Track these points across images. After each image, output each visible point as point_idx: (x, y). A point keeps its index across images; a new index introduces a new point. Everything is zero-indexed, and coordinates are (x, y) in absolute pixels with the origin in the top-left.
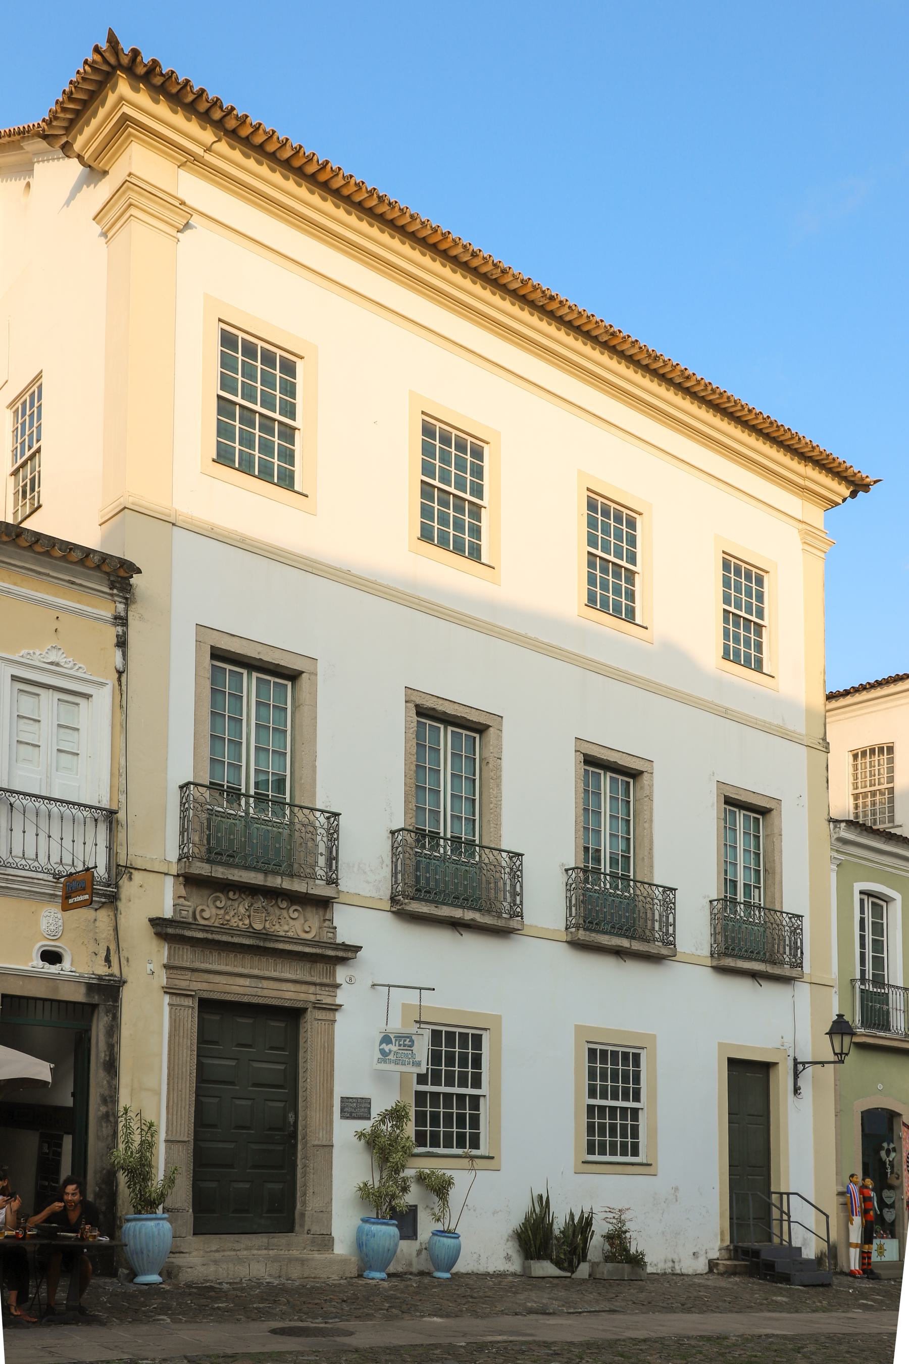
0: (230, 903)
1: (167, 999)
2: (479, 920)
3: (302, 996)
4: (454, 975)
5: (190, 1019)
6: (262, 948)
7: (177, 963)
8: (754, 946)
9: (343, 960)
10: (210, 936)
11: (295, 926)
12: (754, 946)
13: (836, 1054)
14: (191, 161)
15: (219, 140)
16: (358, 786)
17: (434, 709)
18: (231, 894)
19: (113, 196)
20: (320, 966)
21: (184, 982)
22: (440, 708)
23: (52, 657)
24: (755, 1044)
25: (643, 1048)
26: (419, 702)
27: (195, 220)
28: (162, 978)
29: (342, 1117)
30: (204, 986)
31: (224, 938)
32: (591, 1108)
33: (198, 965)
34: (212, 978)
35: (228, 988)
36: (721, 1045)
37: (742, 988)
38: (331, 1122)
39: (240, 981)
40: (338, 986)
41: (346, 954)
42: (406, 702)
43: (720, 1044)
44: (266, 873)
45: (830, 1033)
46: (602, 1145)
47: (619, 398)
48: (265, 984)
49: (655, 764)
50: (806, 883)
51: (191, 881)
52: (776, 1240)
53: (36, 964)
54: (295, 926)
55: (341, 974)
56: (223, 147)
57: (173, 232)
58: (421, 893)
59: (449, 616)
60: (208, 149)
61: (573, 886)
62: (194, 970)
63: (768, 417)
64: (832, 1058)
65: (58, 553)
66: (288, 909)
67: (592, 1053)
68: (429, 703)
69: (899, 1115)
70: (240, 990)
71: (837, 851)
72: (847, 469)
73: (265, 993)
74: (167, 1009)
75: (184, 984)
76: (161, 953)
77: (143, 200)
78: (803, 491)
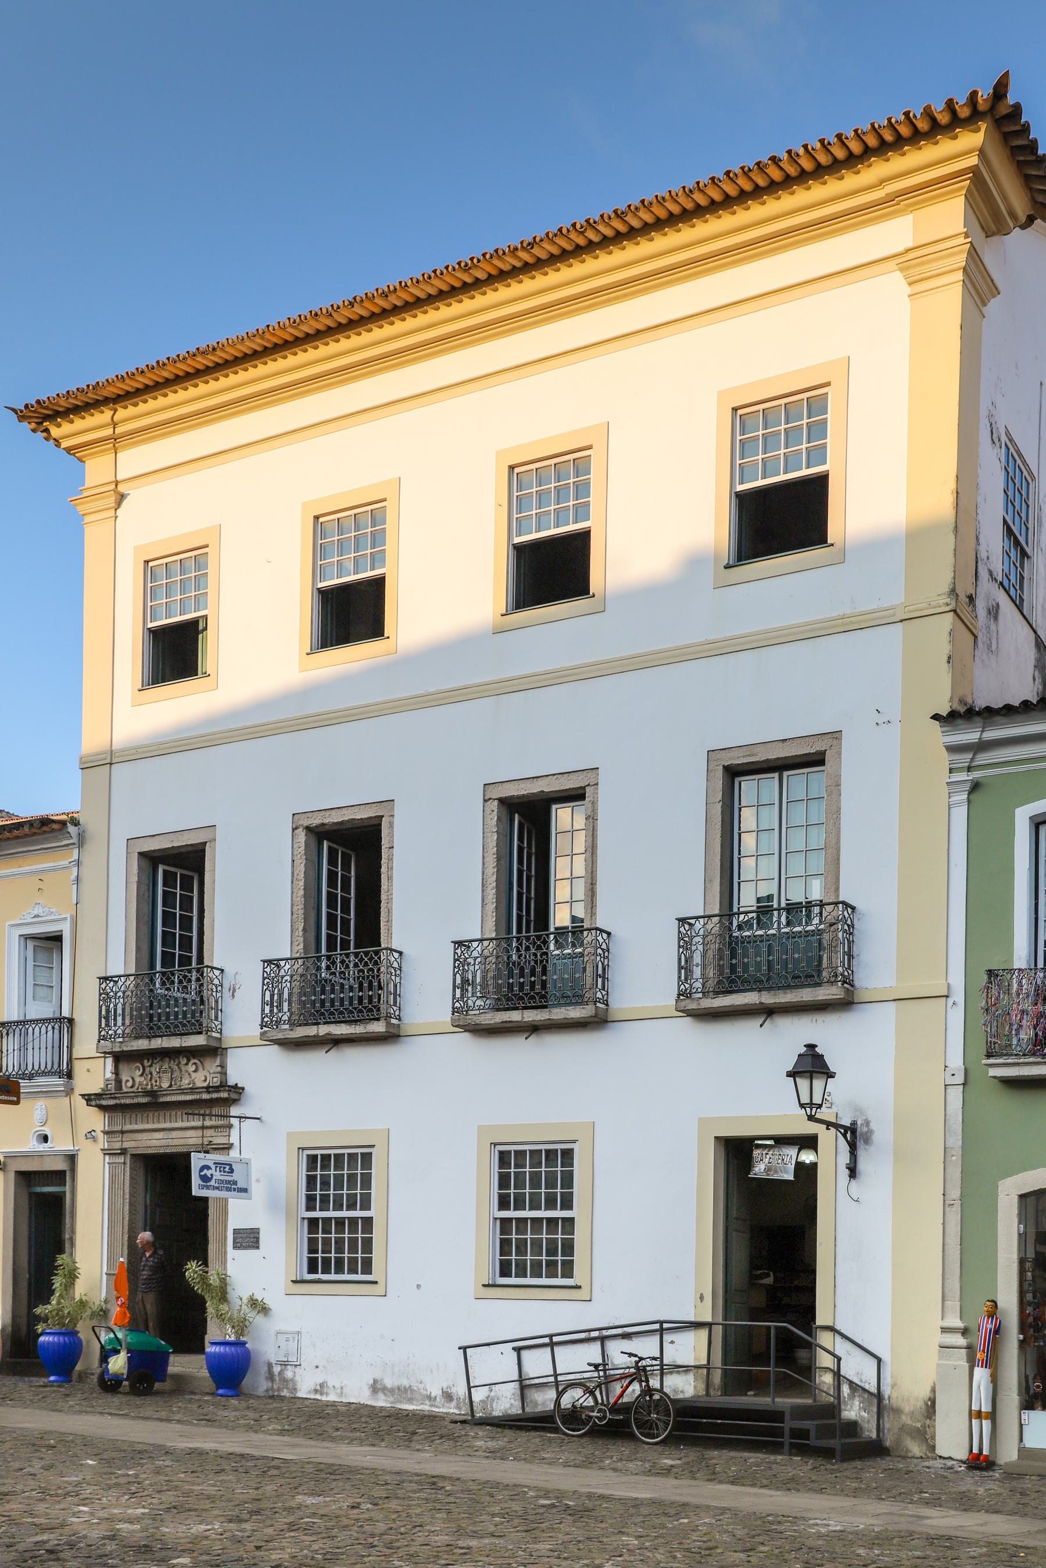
2: (335, 1032)
8: (770, 962)
9: (235, 1101)
10: (118, 1101)
11: (200, 1076)
12: (770, 962)
14: (115, 442)
15: (115, 411)
17: (323, 824)
19: (927, 279)
23: (36, 912)
25: (574, 1142)
26: (306, 823)
28: (102, 1142)
32: (505, 1223)
36: (701, 1121)
38: (226, 1253)
39: (159, 1137)
43: (700, 1120)
44: (149, 1038)
46: (326, 1262)
47: (552, 317)
48: (174, 1134)
51: (119, 1058)
54: (200, 1076)
56: (121, 413)
58: (729, 984)
59: (825, 628)
61: (479, 960)
62: (122, 1132)
63: (88, 386)
67: (504, 1158)
73: (176, 1142)
77: (87, 506)
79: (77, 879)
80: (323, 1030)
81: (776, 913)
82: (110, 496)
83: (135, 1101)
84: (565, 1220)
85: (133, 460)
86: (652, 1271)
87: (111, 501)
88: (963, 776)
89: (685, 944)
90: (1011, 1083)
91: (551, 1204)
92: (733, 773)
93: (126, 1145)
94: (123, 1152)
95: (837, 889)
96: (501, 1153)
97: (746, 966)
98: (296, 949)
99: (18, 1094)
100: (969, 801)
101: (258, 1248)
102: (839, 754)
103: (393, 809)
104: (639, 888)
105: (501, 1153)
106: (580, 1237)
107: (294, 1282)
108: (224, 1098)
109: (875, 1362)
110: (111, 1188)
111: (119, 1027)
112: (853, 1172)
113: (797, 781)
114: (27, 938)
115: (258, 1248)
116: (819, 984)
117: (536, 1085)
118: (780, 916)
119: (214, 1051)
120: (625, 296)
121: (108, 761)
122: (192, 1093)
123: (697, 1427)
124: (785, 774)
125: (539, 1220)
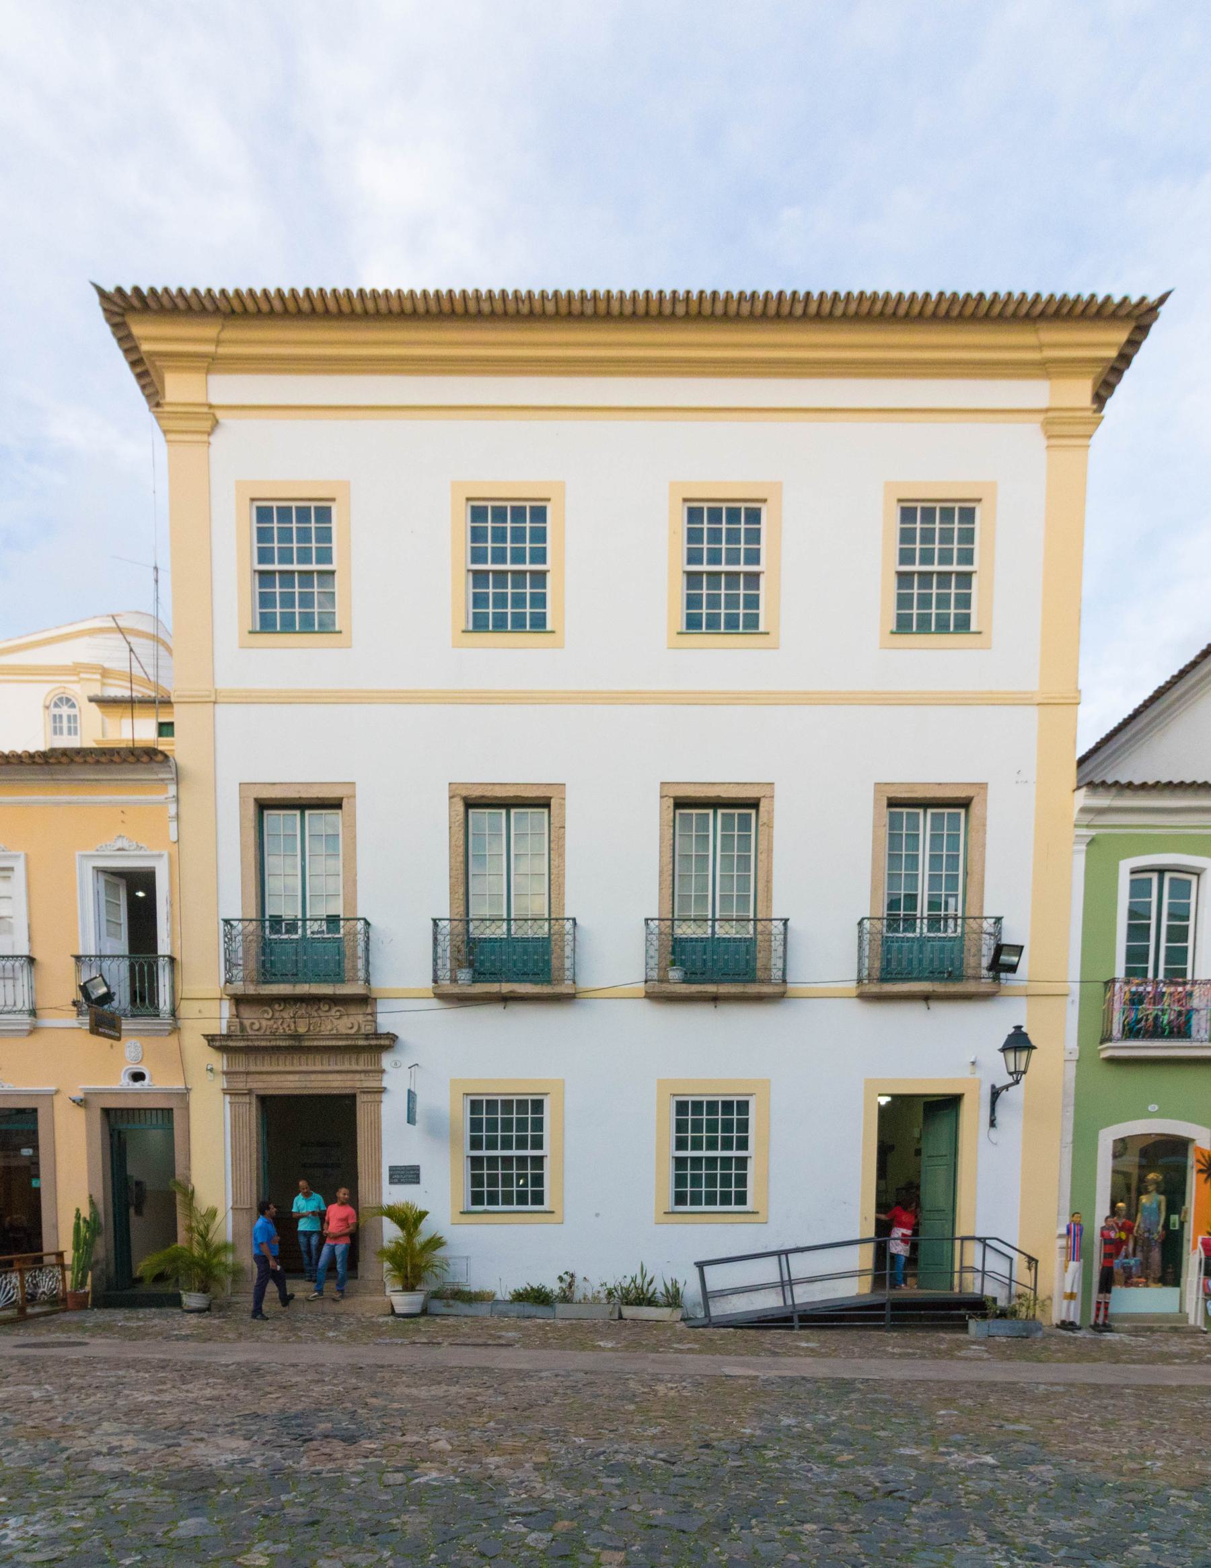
0: (277, 1015)
1: (228, 1098)
3: (349, 1084)
4: (501, 1049)
5: (251, 1113)
6: (297, 1047)
7: (233, 1069)
10: (250, 1043)
11: (343, 1024)
13: (1011, 1074)
14: (212, 364)
16: (397, 891)
17: (483, 797)
18: (276, 1006)
20: (363, 1057)
21: (241, 1084)
22: (489, 794)
23: (119, 844)
24: (927, 1076)
27: (219, 414)
28: (222, 1082)
29: (391, 1183)
30: (260, 1085)
31: (263, 1044)
33: (253, 1068)
34: (264, 1077)
35: (280, 1085)
37: (912, 1014)
38: (380, 1188)
40: (383, 1071)
41: (389, 1042)
42: (662, 797)
45: (1003, 1050)
48: (313, 1077)
49: (776, 787)
50: (1032, 880)
51: (239, 1000)
52: (957, 1290)
53: (125, 1083)
54: (343, 1024)
55: (387, 1060)
57: (205, 438)
60: (218, 342)
62: (248, 1073)
64: (1010, 1080)
65: (116, 758)
66: (329, 1010)
68: (476, 793)
69: (1193, 1140)
70: (292, 1085)
71: (1088, 826)
72: (1006, 304)
74: (228, 1106)
75: (241, 1086)
76: (219, 1062)
78: (1045, 369)
79: (178, 816)
80: (493, 988)
81: (918, 921)
82: (207, 419)
83: (273, 1043)
84: (534, 1158)
85: (224, 388)
86: (814, 1202)
87: (207, 425)
88: (1084, 831)
89: (229, 938)
90: (1112, 1061)
91: (727, 1145)
92: (263, 806)
93: (254, 1085)
94: (250, 1092)
95: (982, 907)
96: (473, 1102)
97: (482, 963)
98: (456, 911)
99: (119, 1031)
100: (1087, 852)
101: (418, 1183)
102: (985, 800)
103: (564, 791)
104: (822, 890)
105: (473, 1102)
106: (751, 1171)
107: (462, 1213)
108: (381, 1044)
109: (1008, 1261)
110: (233, 1127)
111: (238, 973)
112: (992, 1124)
113: (318, 821)
114: (99, 871)
115: (418, 1183)
116: (343, 981)
117: (714, 1048)
118: (922, 923)
119: (364, 1000)
120: (177, 367)
121: (213, 699)
122: (347, 1039)
123: (906, 1318)
124: (307, 812)
125: (699, 1159)
